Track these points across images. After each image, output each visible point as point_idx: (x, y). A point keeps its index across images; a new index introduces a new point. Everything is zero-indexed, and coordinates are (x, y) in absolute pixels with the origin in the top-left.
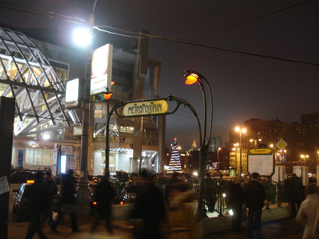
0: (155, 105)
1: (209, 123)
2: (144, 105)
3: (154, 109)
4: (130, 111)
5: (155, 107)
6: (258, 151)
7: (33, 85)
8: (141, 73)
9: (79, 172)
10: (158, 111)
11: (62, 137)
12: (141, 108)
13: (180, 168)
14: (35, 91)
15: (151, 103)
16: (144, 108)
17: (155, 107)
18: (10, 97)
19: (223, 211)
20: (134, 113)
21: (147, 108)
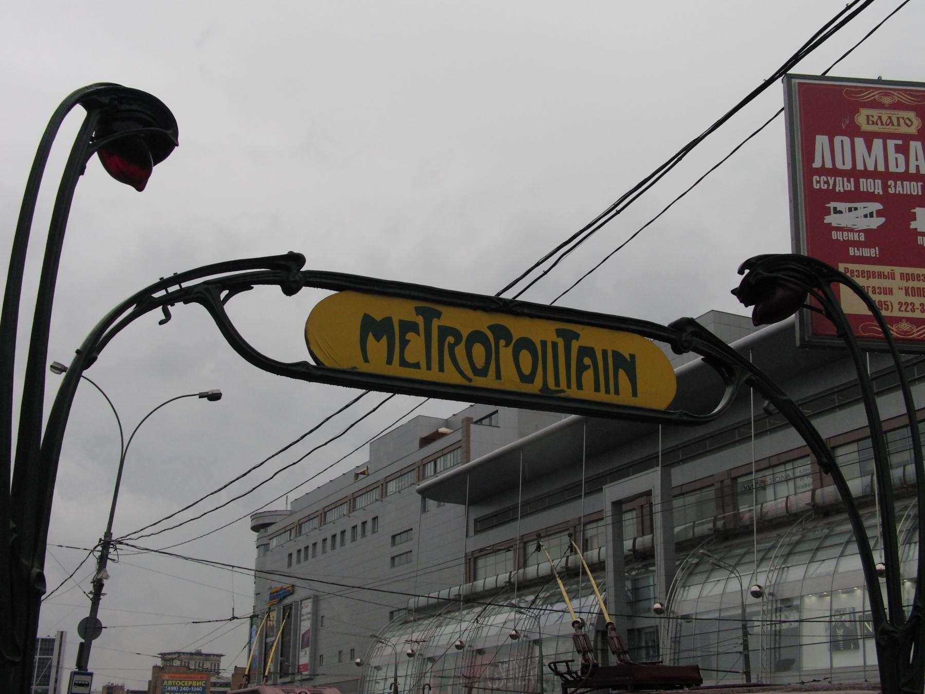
2: (501, 332)
16: (506, 353)
17: (587, 361)
20: (417, 366)
21: (525, 357)
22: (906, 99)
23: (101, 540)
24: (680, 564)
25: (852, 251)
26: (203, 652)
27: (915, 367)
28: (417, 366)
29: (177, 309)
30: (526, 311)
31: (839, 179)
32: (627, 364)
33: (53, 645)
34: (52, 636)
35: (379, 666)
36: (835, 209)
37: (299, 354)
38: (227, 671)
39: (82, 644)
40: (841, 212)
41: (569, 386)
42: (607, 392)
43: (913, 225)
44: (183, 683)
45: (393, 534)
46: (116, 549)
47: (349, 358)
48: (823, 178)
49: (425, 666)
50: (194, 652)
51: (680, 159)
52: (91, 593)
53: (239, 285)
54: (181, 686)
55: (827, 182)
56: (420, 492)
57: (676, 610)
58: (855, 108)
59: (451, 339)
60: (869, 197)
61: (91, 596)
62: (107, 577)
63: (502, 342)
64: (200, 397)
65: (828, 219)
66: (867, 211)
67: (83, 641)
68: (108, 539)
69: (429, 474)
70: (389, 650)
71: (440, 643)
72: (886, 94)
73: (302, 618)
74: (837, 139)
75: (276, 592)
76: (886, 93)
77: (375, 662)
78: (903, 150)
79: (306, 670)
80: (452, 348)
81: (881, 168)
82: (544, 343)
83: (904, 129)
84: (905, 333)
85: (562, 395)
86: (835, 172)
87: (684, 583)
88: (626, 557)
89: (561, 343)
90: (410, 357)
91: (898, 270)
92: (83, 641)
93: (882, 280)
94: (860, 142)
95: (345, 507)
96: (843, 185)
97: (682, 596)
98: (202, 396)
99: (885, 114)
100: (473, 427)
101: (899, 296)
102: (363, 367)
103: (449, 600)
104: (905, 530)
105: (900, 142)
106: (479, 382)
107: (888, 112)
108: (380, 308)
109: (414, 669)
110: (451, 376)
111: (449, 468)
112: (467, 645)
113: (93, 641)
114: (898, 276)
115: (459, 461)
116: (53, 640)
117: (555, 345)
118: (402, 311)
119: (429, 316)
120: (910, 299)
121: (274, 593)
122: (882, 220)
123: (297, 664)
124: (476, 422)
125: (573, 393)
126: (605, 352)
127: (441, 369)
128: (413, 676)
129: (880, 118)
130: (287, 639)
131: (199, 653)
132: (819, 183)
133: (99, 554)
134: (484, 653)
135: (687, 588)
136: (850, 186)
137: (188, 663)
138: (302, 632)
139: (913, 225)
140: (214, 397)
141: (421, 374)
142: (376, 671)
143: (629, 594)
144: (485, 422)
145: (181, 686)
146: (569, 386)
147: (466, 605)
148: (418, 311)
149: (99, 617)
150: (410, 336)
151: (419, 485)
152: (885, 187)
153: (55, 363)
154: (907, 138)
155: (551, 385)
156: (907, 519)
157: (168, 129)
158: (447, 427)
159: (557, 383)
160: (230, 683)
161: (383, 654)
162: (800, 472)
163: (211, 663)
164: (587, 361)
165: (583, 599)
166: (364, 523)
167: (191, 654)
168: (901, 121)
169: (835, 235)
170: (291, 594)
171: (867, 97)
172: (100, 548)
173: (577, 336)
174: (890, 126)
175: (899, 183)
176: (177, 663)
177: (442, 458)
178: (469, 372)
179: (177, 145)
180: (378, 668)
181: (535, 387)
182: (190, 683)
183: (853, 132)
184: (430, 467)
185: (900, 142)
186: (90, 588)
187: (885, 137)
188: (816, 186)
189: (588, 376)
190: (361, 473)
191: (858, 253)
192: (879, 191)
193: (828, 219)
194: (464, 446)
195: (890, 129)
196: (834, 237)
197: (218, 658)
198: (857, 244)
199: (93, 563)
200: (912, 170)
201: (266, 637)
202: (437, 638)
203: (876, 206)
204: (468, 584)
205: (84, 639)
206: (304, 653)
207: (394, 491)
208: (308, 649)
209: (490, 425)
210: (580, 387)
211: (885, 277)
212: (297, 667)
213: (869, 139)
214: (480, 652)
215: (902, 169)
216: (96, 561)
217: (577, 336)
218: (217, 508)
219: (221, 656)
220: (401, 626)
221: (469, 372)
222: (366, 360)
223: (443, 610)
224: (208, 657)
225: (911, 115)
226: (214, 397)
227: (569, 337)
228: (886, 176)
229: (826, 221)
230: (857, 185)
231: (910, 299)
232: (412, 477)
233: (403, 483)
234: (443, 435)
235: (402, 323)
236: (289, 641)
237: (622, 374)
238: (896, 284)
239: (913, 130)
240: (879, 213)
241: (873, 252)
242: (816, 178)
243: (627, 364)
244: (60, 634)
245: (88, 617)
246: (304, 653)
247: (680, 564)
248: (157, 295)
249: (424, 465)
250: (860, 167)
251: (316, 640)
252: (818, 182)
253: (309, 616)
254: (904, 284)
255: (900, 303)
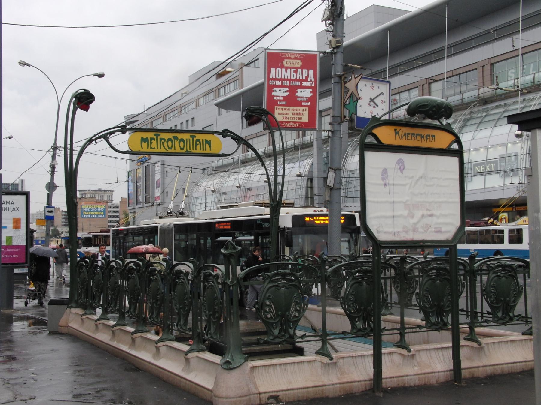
0: (198, 140)
1: (280, 173)
2: (175, 138)
7: (68, 235)
9: (221, 275)
13: (327, 220)
14: (422, 320)
15: (191, 136)
16: (177, 143)
17: (198, 143)
18: (372, 136)
20: (154, 148)
21: (182, 143)
22: (298, 56)
23: (52, 146)
24: (350, 144)
25: (279, 103)
26: (102, 189)
27: (473, 41)
28: (154, 148)
29: (99, 140)
30: (182, 132)
31: (277, 81)
32: (209, 143)
33: (18, 187)
34: (17, 182)
35: (197, 197)
36: (275, 90)
37: (127, 149)
38: (116, 200)
39: (48, 194)
40: (276, 91)
41: (193, 150)
42: (203, 150)
43: (296, 95)
44: (93, 207)
45: (203, 127)
46: (59, 151)
47: (137, 148)
48: (273, 81)
49: (221, 197)
50: (97, 189)
51: (262, 39)
52: (50, 171)
53: (111, 133)
54: (92, 208)
55: (273, 82)
56: (217, 105)
57: (347, 168)
58: (283, 59)
59: (163, 141)
60: (285, 86)
61: (50, 172)
62: (57, 164)
63: (176, 140)
64: (94, 76)
65: (273, 94)
66: (284, 91)
67: (49, 193)
68: (55, 146)
69: (222, 95)
70: (202, 189)
71: (229, 185)
72: (292, 55)
73: (156, 172)
74: (277, 69)
75: (141, 158)
76: (292, 54)
77: (195, 195)
78: (296, 72)
79: (159, 200)
80: (163, 143)
81: (289, 78)
82: (187, 139)
83: (297, 66)
84: (291, 125)
85: (191, 152)
86: (276, 79)
87: (352, 153)
88: (324, 140)
89: (191, 139)
90: (153, 147)
91: (291, 108)
92: (49, 193)
93: (286, 111)
94: (284, 70)
95: (176, 112)
96: (278, 83)
97: (351, 160)
98: (95, 75)
99: (291, 61)
100: (244, 67)
101: (291, 115)
102: (142, 150)
103: (234, 163)
104: (458, 127)
105: (295, 70)
106: (170, 151)
107: (292, 60)
108: (145, 135)
109: (215, 199)
110: (163, 150)
111: (233, 91)
112: (242, 186)
113: (53, 193)
114: (291, 109)
115: (238, 87)
116: (18, 184)
117: (190, 139)
118: (151, 135)
119: (157, 135)
120: (293, 116)
121: (139, 159)
122: (288, 93)
123: (154, 197)
124: (246, 65)
125: (194, 151)
126: (203, 140)
127: (160, 148)
128: (215, 202)
129: (290, 62)
130: (148, 183)
131: (100, 190)
132: (271, 82)
133: (52, 153)
134: (252, 190)
135: (353, 156)
136: (280, 84)
137: (95, 195)
138: (156, 180)
139: (296, 95)
140: (101, 76)
141: (156, 150)
142: (196, 199)
143: (325, 159)
144: (252, 65)
145: (92, 208)
146: (193, 150)
147: (243, 165)
148: (155, 135)
149: (55, 182)
150: (153, 141)
151: (216, 100)
152: (290, 83)
153: (21, 61)
154: (297, 68)
155: (188, 150)
156: (459, 122)
157: (92, 98)
158: (231, 68)
159: (190, 149)
160: (119, 206)
161: (199, 192)
162: (413, 96)
163: (108, 196)
164: (198, 143)
165: (301, 163)
166: (187, 121)
167: (96, 191)
168: (296, 63)
169: (275, 98)
170: (149, 159)
171: (287, 56)
172: (52, 150)
173: (195, 137)
174: (293, 65)
175: (294, 82)
176: (88, 196)
177: (228, 85)
178: (167, 149)
179: (95, 101)
180: (197, 198)
181: (184, 151)
182: (97, 206)
183: (282, 67)
184: (222, 90)
185: (295, 70)
186: (49, 169)
187: (291, 68)
188: (270, 84)
189: (198, 147)
190: (184, 93)
191: (280, 103)
192: (288, 85)
193: (273, 94)
194: (240, 79)
195: (293, 66)
196: (274, 99)
197: (111, 193)
198: (280, 101)
199: (49, 156)
200: (298, 78)
201: (137, 182)
202: (227, 183)
203: (287, 89)
204: (243, 154)
205: (49, 191)
206: (158, 190)
207: (203, 103)
208: (160, 189)
209: (255, 67)
210: (196, 149)
211: (287, 110)
212: (154, 198)
213: (286, 68)
214: (249, 189)
215: (295, 78)
216: (51, 156)
217: (195, 137)
218: (95, 27)
219: (113, 191)
220: (208, 176)
221: (167, 149)
222: (142, 148)
223: (230, 168)
224: (106, 192)
225: (299, 61)
226: (101, 76)
227: (193, 137)
228: (290, 80)
229: (272, 94)
230: (282, 83)
231: (293, 116)
232: (212, 95)
233: (208, 99)
234: (229, 72)
235: (151, 138)
236: (149, 185)
237: (207, 145)
238: (290, 112)
239: (299, 66)
240: (287, 91)
241: (284, 103)
242: (270, 81)
243: (209, 143)
244: (21, 181)
245: (50, 182)
246: (158, 190)
247: (350, 144)
248: (93, 139)
249: (219, 89)
250: (283, 77)
251: (164, 184)
252: (271, 82)
253: (160, 171)
254: (292, 112)
255: (291, 117)
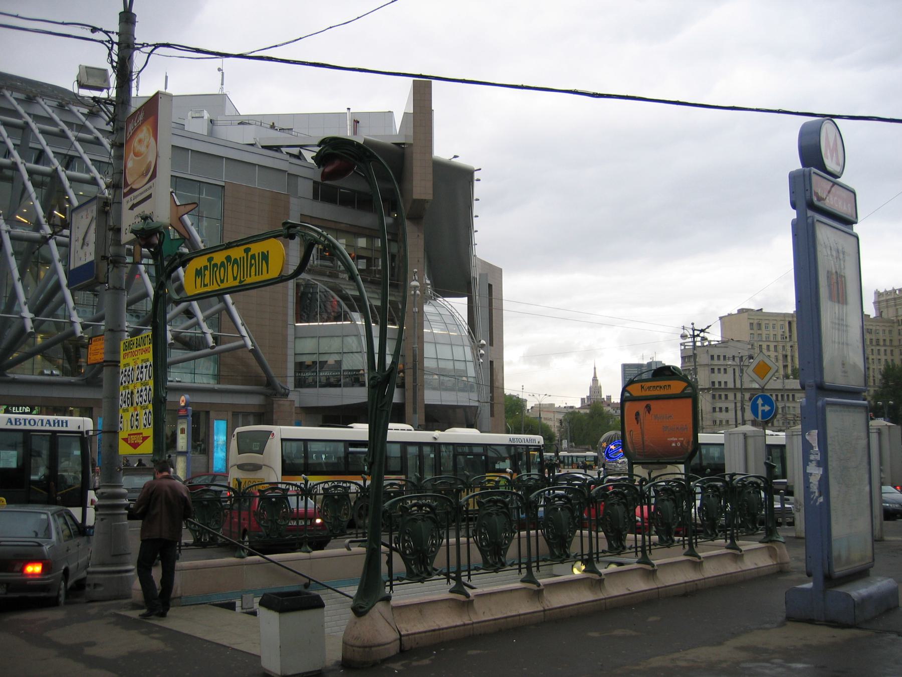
3: (253, 268)
4: (199, 281)
5: (253, 262)
6: (649, 388)
8: (414, 81)
10: (262, 274)
11: (333, 314)
12: (222, 269)
17: (253, 262)
19: (538, 567)
